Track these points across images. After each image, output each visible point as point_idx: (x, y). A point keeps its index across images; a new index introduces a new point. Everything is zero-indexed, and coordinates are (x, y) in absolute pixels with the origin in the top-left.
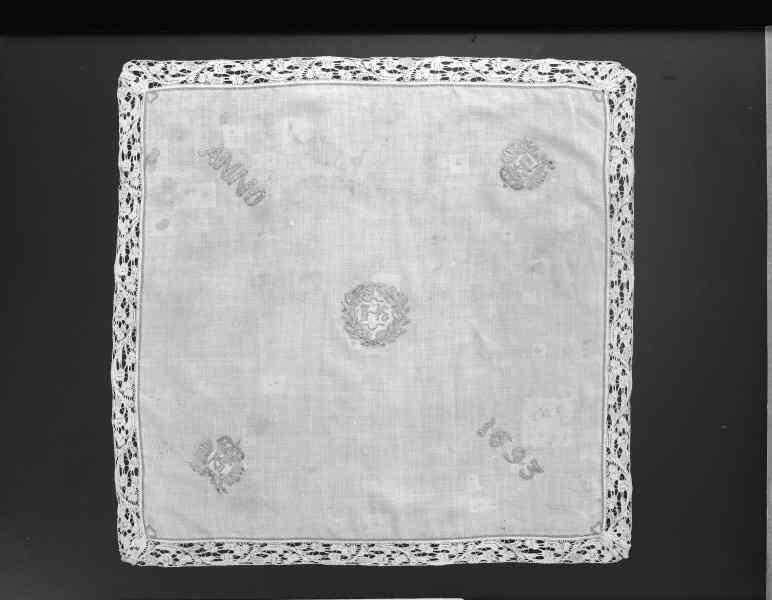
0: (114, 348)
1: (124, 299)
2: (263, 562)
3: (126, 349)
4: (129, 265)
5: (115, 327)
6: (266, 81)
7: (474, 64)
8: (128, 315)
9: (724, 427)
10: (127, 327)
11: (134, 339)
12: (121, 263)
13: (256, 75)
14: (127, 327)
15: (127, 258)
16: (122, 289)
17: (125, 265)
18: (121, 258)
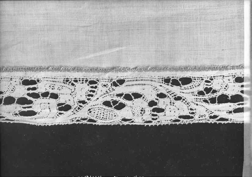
0: (206, 120)
1: (107, 103)
2: (115, 118)
3: (207, 96)
4: (36, 96)
5: (164, 119)
6: (167, 81)
7: (186, 113)
8: (137, 96)
9: (165, 167)
10: (162, 96)
11: (187, 81)
12: (33, 113)
13: (187, 93)
14: (162, 96)
15: (22, 101)
16: (86, 107)
17: (37, 105)
18: (23, 114)
